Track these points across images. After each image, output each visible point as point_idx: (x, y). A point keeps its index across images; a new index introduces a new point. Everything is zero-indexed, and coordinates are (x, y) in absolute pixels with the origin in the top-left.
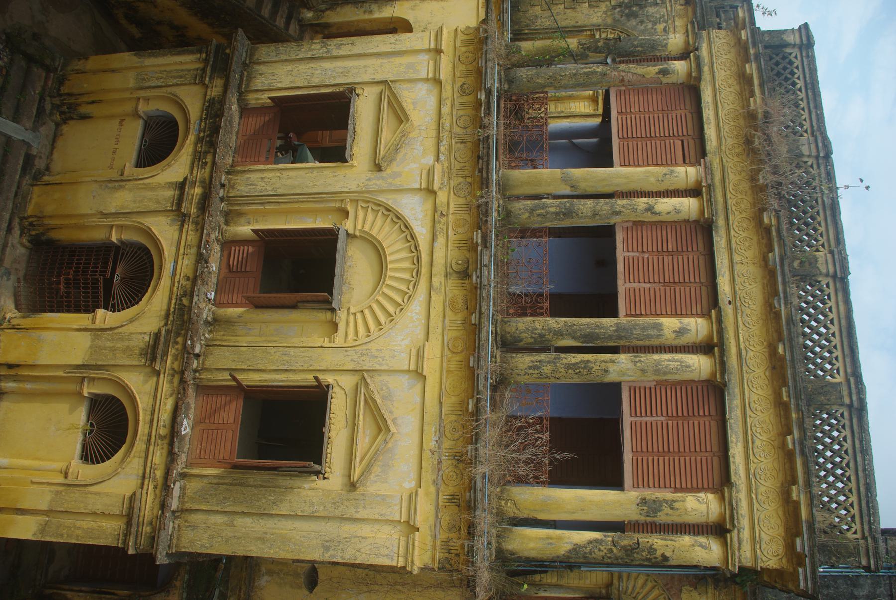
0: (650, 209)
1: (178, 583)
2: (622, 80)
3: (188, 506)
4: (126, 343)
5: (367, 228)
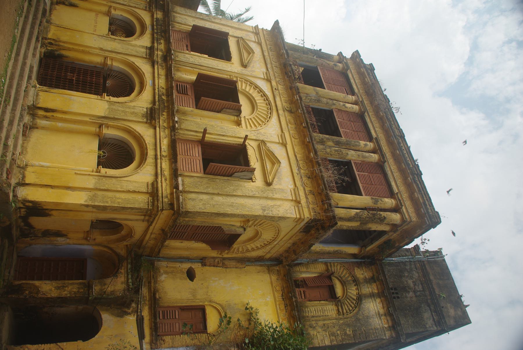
0: (344, 105)
1: (123, 271)
2: (322, 64)
3: (187, 189)
4: (133, 110)
5: (243, 88)
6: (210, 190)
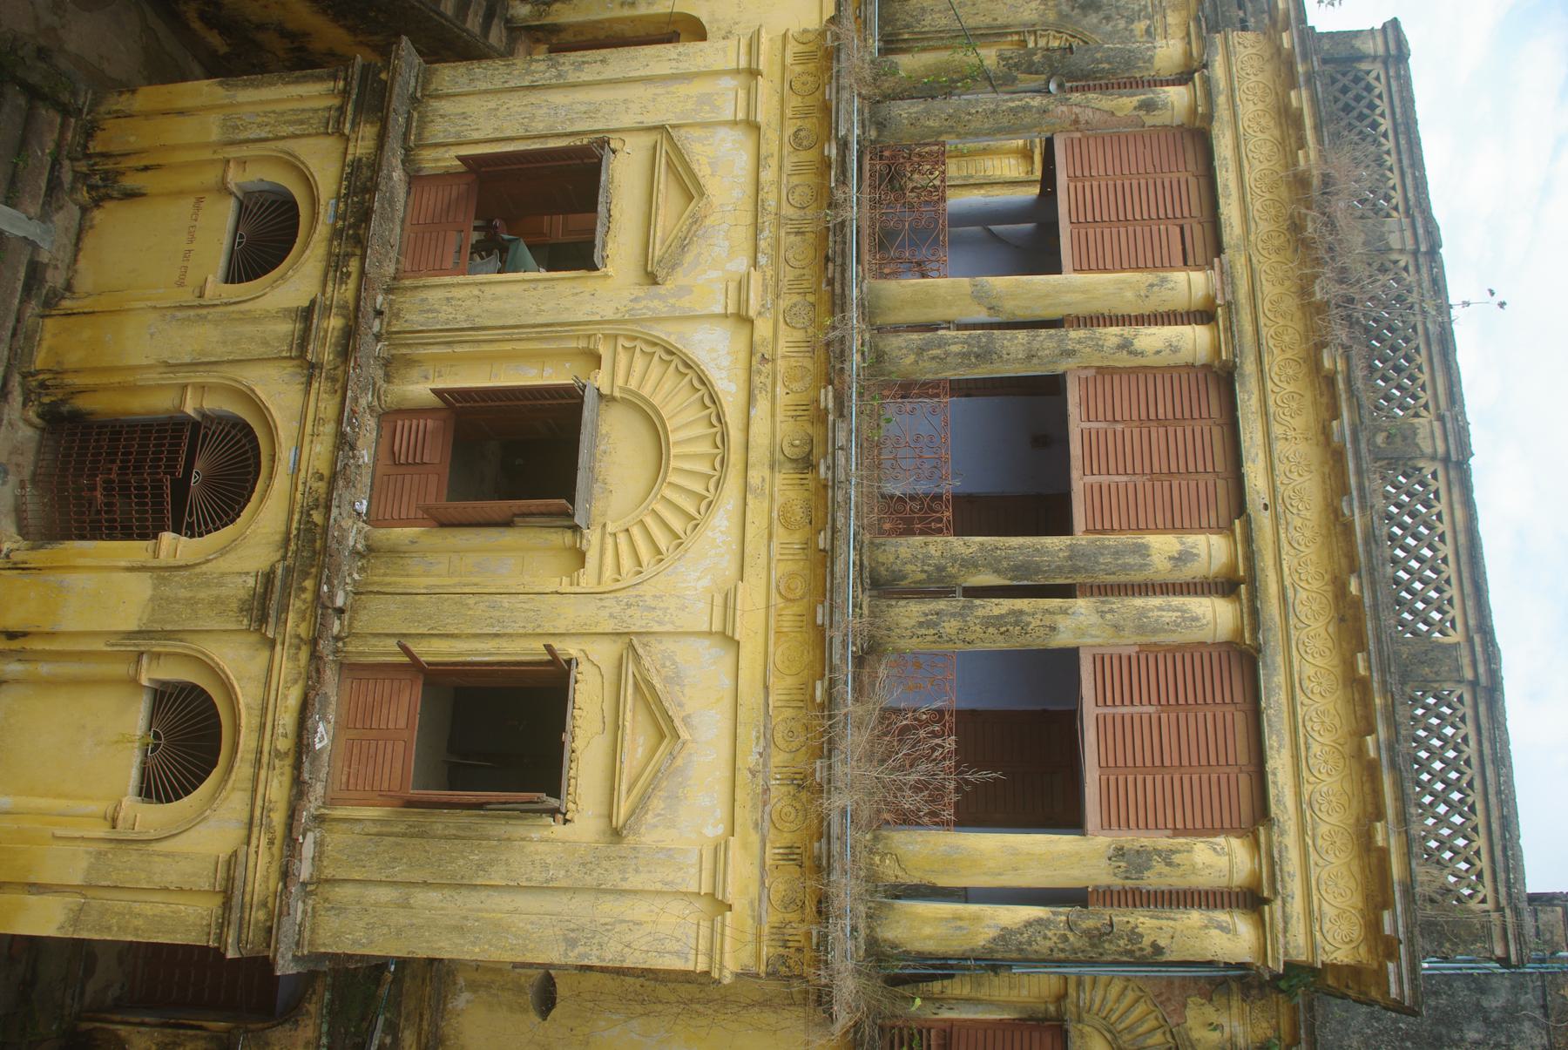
3: (329, 872)
4: (215, 592)
5: (633, 385)
6: (400, 872)
